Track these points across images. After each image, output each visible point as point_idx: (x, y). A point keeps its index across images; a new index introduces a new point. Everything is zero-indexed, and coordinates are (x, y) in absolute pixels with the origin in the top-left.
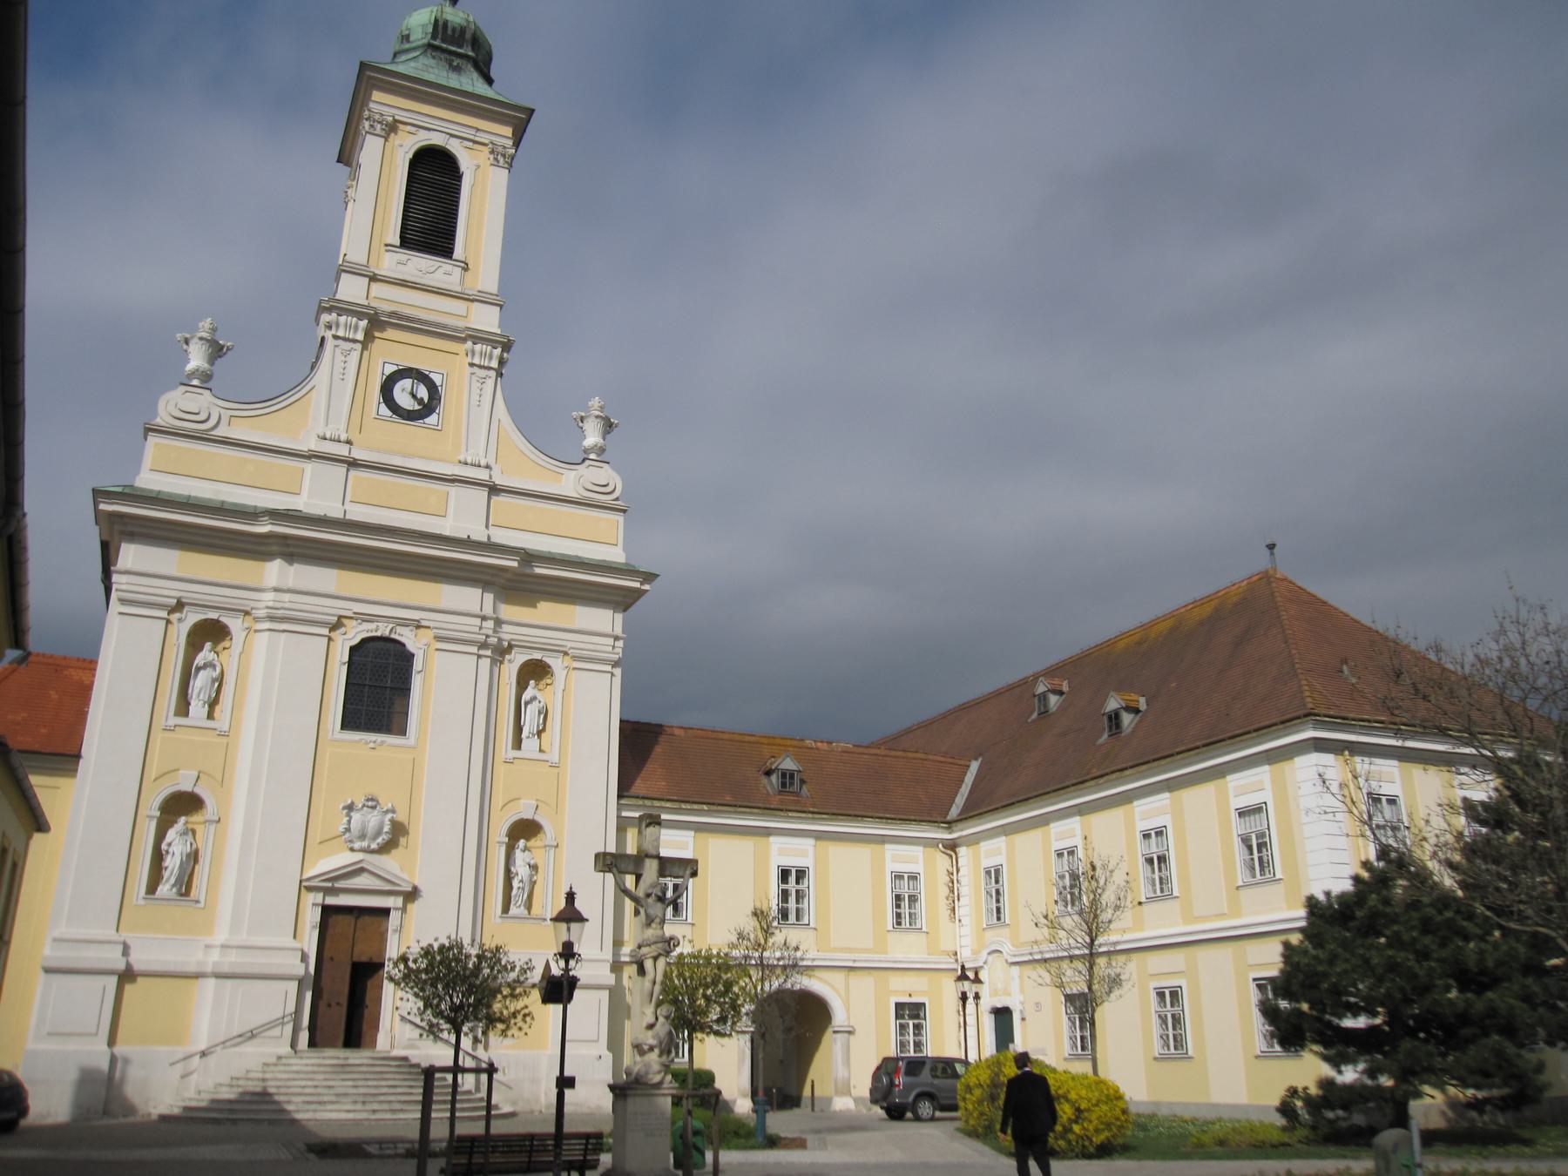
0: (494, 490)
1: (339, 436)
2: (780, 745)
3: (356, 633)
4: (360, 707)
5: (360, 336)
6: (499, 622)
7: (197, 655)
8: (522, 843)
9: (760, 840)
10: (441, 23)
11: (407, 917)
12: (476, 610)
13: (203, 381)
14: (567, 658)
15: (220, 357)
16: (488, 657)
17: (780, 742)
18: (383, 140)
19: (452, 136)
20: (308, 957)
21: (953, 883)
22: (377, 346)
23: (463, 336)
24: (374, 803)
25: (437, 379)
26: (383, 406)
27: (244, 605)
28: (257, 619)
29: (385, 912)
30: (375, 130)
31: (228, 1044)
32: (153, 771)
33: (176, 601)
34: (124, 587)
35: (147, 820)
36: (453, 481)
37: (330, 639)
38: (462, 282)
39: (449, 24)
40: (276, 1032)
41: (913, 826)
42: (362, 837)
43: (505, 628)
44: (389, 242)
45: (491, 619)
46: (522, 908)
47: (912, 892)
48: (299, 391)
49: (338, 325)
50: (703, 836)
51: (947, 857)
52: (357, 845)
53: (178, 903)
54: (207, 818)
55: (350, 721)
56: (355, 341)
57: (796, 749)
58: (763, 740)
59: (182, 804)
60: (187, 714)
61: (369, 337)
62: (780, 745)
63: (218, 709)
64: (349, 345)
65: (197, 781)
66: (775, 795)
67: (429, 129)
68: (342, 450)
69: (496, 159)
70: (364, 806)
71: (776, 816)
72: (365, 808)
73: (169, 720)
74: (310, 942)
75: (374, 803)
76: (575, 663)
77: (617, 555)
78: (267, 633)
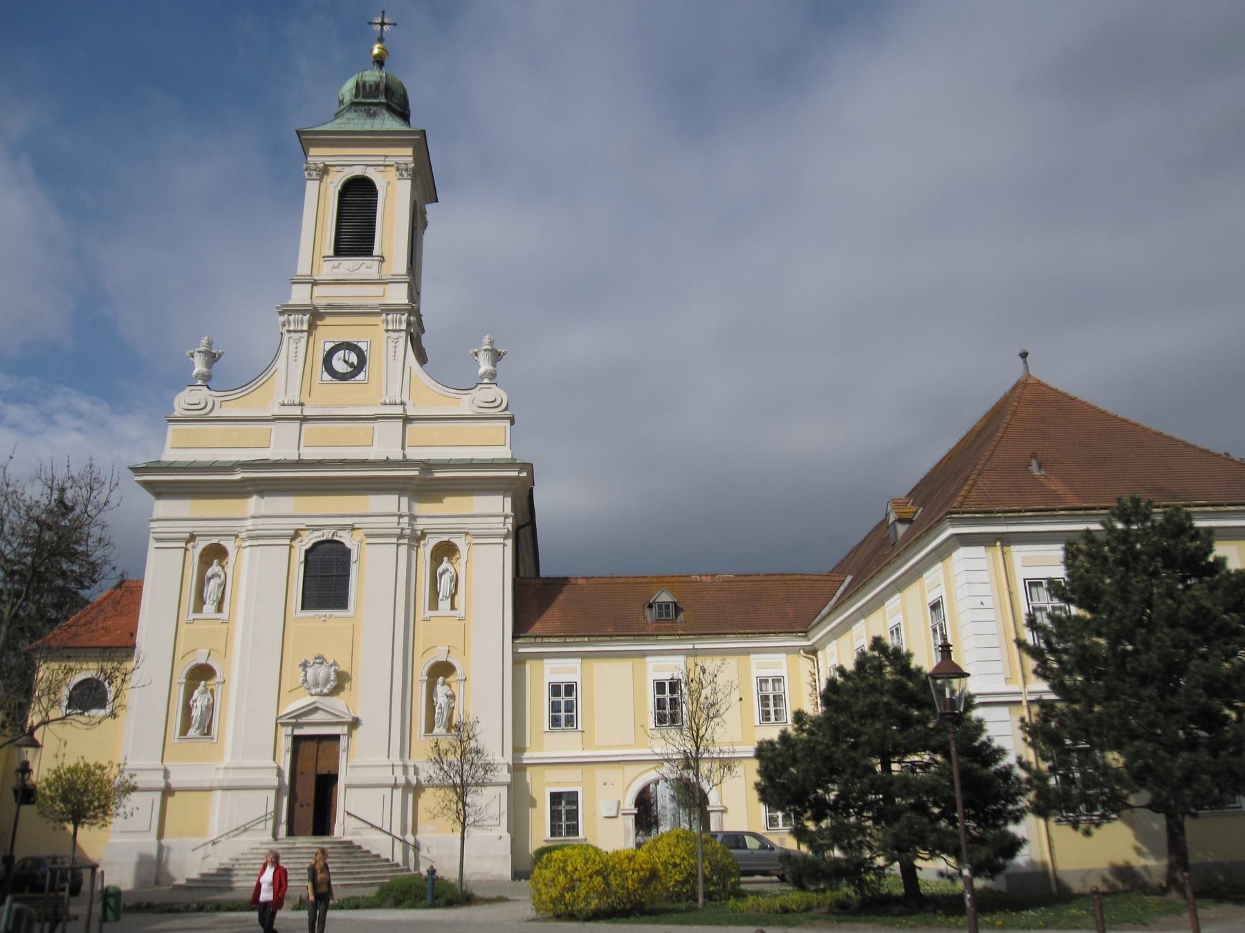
0: (407, 420)
1: (395, 401)
2: (668, 582)
3: (308, 540)
4: (330, 592)
5: (305, 327)
6: (413, 518)
7: (207, 570)
8: (441, 679)
9: (637, 661)
10: (361, 85)
11: (353, 741)
12: (395, 511)
13: (490, 379)
14: (468, 537)
15: (215, 361)
16: (405, 544)
17: (669, 579)
18: (318, 182)
19: (368, 165)
20: (284, 772)
21: (815, 681)
22: (320, 332)
23: (379, 311)
24: (321, 660)
25: (363, 346)
26: (325, 374)
27: (235, 531)
28: (243, 540)
29: (336, 738)
30: (312, 176)
31: (230, 835)
32: (180, 652)
33: (188, 534)
34: (157, 530)
35: (179, 685)
36: (273, 420)
37: (291, 547)
38: (380, 271)
39: (367, 84)
40: (262, 826)
41: (772, 637)
42: (316, 685)
43: (419, 521)
44: (325, 255)
45: (406, 516)
46: (441, 727)
47: (777, 693)
48: (267, 373)
49: (289, 323)
50: (587, 662)
51: (809, 661)
52: (313, 691)
53: (201, 740)
54: (458, 678)
55: (308, 603)
56: (302, 331)
57: (681, 584)
58: (655, 580)
59: (202, 673)
60: (437, 608)
61: (312, 326)
62: (668, 582)
63: (456, 597)
64: (298, 335)
65: (209, 655)
66: (652, 623)
67: (351, 165)
68: (296, 411)
69: (401, 175)
70: (314, 663)
71: (703, 639)
72: (316, 665)
73: (426, 613)
74: (285, 762)
75: (321, 660)
76: (369, 539)
77: (504, 453)
78: (249, 548)
